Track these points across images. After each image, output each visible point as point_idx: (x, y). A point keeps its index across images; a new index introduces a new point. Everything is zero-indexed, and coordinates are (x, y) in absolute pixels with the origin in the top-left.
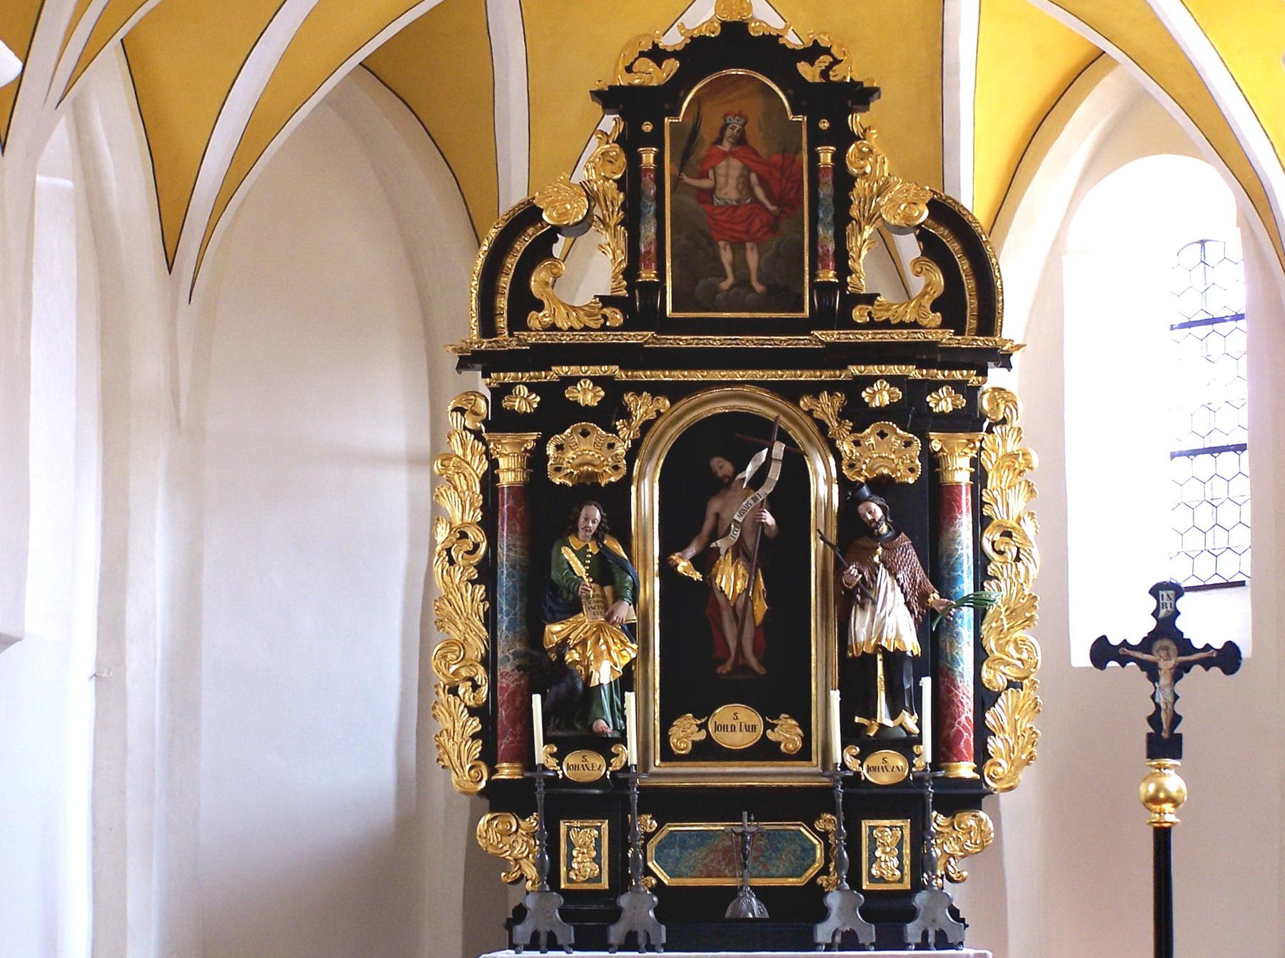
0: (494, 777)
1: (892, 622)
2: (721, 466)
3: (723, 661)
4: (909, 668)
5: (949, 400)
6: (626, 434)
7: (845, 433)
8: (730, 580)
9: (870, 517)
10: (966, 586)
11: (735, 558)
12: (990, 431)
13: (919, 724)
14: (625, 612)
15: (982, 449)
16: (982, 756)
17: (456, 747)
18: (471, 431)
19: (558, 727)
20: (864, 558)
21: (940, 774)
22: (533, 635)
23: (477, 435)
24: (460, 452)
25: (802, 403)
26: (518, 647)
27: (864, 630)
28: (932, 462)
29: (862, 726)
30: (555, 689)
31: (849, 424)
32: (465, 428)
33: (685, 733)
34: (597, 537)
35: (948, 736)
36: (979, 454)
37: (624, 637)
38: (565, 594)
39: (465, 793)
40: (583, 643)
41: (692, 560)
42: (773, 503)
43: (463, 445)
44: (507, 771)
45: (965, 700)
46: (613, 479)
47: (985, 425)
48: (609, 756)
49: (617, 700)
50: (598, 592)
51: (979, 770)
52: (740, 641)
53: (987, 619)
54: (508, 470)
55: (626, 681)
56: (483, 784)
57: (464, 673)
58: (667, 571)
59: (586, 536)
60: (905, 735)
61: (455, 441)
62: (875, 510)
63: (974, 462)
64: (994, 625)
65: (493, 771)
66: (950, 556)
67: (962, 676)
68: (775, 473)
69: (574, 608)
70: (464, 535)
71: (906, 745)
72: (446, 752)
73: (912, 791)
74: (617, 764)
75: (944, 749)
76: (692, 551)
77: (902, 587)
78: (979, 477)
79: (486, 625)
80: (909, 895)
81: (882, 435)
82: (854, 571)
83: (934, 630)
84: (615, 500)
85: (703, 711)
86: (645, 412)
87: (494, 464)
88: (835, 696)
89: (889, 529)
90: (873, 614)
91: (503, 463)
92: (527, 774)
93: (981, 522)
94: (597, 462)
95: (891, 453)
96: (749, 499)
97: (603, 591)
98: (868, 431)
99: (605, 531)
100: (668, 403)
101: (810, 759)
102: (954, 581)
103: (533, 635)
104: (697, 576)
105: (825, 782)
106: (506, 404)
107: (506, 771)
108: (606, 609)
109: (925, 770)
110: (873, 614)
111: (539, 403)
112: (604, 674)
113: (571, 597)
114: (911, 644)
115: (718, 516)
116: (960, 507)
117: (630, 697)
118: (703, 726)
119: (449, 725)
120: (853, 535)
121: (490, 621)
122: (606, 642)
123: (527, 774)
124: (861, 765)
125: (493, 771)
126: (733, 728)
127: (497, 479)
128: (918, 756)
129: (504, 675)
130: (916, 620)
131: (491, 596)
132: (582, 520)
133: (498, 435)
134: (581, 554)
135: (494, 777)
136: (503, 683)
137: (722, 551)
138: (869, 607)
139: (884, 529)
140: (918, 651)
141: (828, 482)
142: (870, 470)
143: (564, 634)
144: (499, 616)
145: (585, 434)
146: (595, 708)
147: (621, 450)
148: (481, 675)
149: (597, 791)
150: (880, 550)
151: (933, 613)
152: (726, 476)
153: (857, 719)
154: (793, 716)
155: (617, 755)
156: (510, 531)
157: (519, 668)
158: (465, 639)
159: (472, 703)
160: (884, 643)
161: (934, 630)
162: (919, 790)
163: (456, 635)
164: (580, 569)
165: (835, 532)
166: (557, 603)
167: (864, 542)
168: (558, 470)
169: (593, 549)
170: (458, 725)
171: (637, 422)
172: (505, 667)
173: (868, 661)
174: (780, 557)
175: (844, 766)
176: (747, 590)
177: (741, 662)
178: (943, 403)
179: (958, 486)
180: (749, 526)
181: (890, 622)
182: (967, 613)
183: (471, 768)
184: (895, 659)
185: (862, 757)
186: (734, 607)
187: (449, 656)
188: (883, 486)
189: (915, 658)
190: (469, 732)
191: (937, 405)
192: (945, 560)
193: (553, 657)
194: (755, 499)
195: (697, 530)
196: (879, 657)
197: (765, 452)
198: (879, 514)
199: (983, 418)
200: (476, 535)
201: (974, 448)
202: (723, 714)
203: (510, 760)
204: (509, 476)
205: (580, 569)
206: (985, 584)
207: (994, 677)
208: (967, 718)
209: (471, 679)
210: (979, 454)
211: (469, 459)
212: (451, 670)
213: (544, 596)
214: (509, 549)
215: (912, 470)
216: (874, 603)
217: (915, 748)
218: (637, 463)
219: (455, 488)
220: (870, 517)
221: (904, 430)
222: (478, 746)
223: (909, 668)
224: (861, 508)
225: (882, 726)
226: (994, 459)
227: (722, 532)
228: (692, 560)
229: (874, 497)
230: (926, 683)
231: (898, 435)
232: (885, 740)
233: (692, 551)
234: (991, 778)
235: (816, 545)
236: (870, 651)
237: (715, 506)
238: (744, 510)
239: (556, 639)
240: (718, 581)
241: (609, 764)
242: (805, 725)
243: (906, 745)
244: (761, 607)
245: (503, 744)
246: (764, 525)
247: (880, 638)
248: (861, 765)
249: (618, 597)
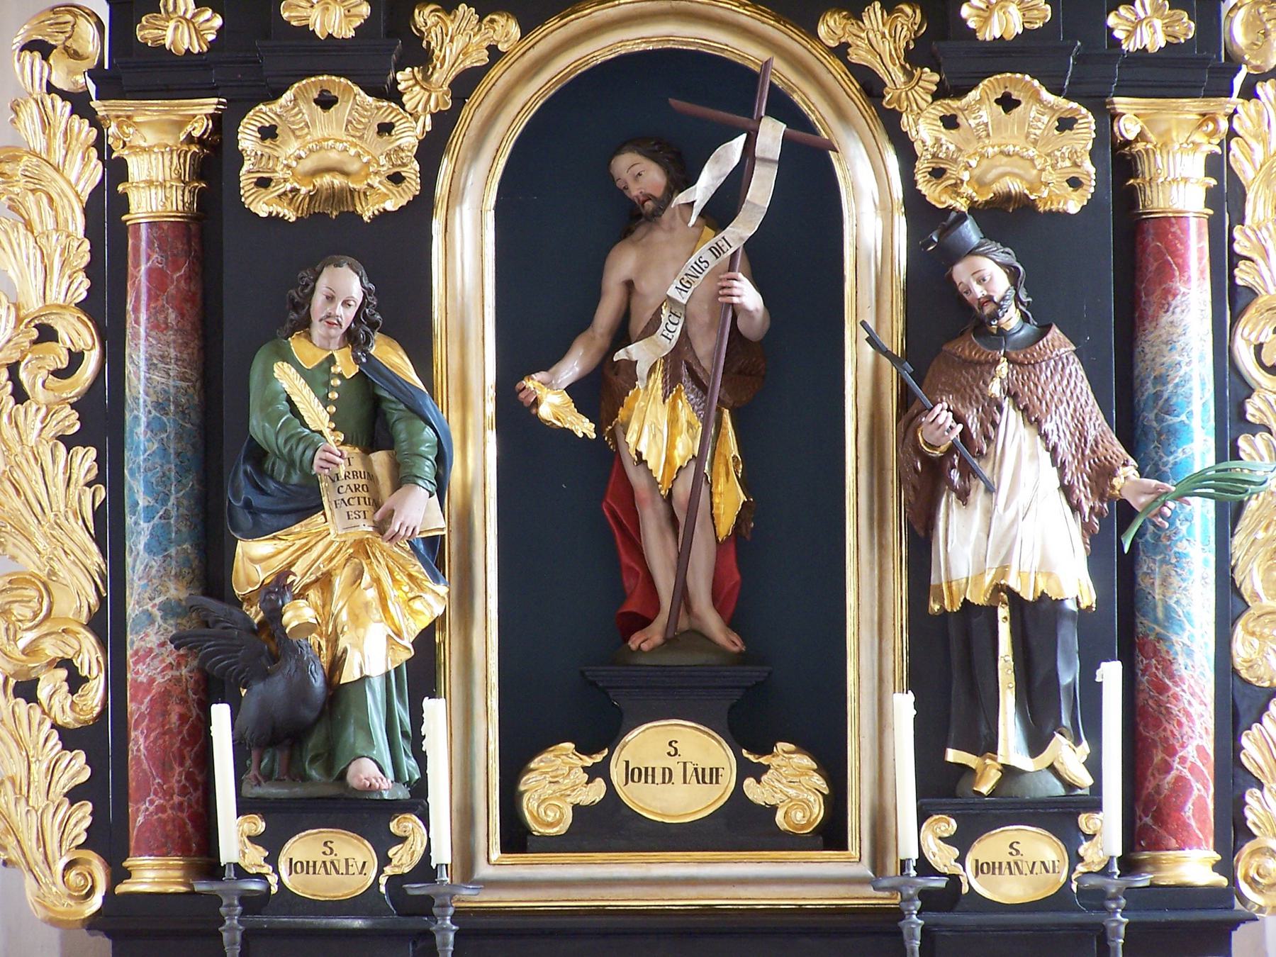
0: (121, 889)
1: (1021, 533)
2: (639, 174)
3: (643, 622)
4: (1069, 637)
5: (1158, 23)
6: (421, 96)
7: (923, 98)
8: (660, 433)
9: (979, 291)
10: (1197, 448)
11: (672, 381)
12: (1249, 92)
13: (1094, 764)
14: (420, 511)
15: (1232, 133)
16: (1233, 832)
17: (34, 819)
18: (65, 95)
19: (268, 777)
20: (966, 381)
21: (1143, 881)
22: (210, 569)
23: (79, 103)
24: (38, 143)
25: (822, 30)
26: (175, 592)
27: (968, 551)
28: (1120, 164)
29: (963, 769)
30: (259, 687)
31: (930, 78)
32: (51, 88)
33: (558, 784)
34: (354, 339)
35: (1158, 789)
36: (1226, 144)
37: (417, 569)
38: (281, 468)
39: (54, 922)
40: (325, 582)
41: (570, 390)
42: (760, 259)
43: (46, 124)
44: (149, 875)
45: (1195, 709)
46: (391, 206)
47: (1238, 81)
48: (383, 843)
49: (402, 713)
50: (357, 466)
51: (1225, 867)
52: (683, 572)
53: (1243, 523)
54: (150, 183)
55: (421, 673)
56: (96, 902)
57: (51, 649)
58: (515, 417)
59: (329, 338)
60: (1060, 790)
61: (30, 114)
62: (988, 275)
63: (1215, 165)
64: (1261, 535)
65: (118, 874)
66: (1161, 380)
67: (1190, 654)
68: (761, 190)
69: (304, 503)
70: (47, 334)
71: (1063, 815)
72: (11, 830)
73: (1075, 917)
74: (403, 859)
75: (1148, 823)
76: (571, 368)
77: (1054, 451)
78: (1227, 198)
79: (98, 539)
80: (394, 808)
81: (1008, 103)
82: (945, 418)
83: (1124, 549)
84: (396, 253)
85: (599, 735)
86: (464, 52)
87: (116, 170)
88: (904, 707)
89: (1025, 318)
90: (989, 514)
91: (137, 168)
92: (201, 887)
93: (1231, 300)
94: (354, 166)
95: (1027, 147)
96: (703, 252)
97: (368, 464)
98: (973, 95)
99: (373, 325)
100: (515, 31)
101: (842, 845)
102: (1169, 436)
103: (210, 569)
104: (584, 427)
105: (867, 897)
106: (146, 32)
107: (152, 875)
108: (377, 505)
109: (1105, 872)
110: (989, 514)
111: (220, 31)
112: (372, 655)
113: (295, 478)
114: (1074, 584)
115: (629, 285)
116: (1183, 268)
117: (434, 709)
118: (599, 772)
119: (18, 769)
120: (941, 326)
121: (109, 528)
122: (377, 581)
123: (201, 887)
124: (961, 860)
125: (118, 874)
126: (668, 775)
127: (122, 203)
128: (1090, 837)
129: (141, 657)
130: (1086, 527)
131: (111, 473)
132: (319, 299)
133: (127, 106)
134: (318, 378)
135: (121, 889)
136: (138, 672)
137: (642, 369)
138: (978, 497)
139: (1011, 319)
140: (1089, 598)
141: (885, 209)
142: (981, 183)
143: (277, 564)
144: (129, 520)
145: (326, 102)
146: (352, 734)
147: (409, 135)
148: (89, 654)
149: (358, 923)
150: (1003, 368)
151: (1126, 512)
152: (649, 197)
153: (952, 755)
154: (804, 746)
155: (402, 840)
156: (157, 326)
157: (178, 641)
158: (52, 572)
159: (68, 719)
160: (1013, 582)
161: (1124, 549)
162: (1093, 916)
163: (30, 563)
164: (317, 415)
165: (899, 326)
166: (263, 492)
167: (968, 348)
168: (263, 183)
169: (346, 366)
170: (39, 770)
171: (443, 75)
172: (148, 637)
173: (975, 620)
174: (773, 383)
175: (924, 867)
176: (698, 459)
177: (683, 624)
178: (1146, 31)
179: (1180, 218)
180: (702, 315)
181: (1025, 530)
182: (1202, 511)
183: (70, 865)
184: (1036, 618)
185: (962, 841)
186: (669, 498)
187: (17, 610)
188: (1008, 218)
189: (1083, 615)
190: (64, 782)
191: (1131, 34)
192: (1150, 389)
193: (255, 614)
194: (716, 251)
195: (584, 322)
196: (1003, 612)
197: (740, 141)
198: (1000, 284)
199: (1234, 64)
200: (77, 333)
201: (1216, 131)
202: (645, 743)
203: (160, 851)
204: (155, 192)
205: (317, 415)
206: (1241, 442)
207: (1264, 656)
208: (1200, 749)
209: (66, 663)
210: (1226, 144)
211: (57, 157)
212: (22, 644)
213: (231, 476)
214: (151, 366)
215: (1075, 183)
216: (990, 490)
217: (1082, 819)
218: (446, 166)
219: (28, 225)
220: (979, 291)
221: (1057, 91)
222: (83, 814)
223: (1069, 637)
224: (961, 272)
225: (1009, 772)
226: (1259, 156)
227: (638, 325)
228: (570, 390)
229: (992, 246)
230: (1111, 674)
231: (1042, 106)
232: (1012, 805)
233: (571, 368)
234: (1253, 883)
235: (858, 359)
236: (979, 598)
237: (623, 264)
238: (687, 274)
239: (262, 575)
240: (631, 438)
241: (384, 861)
242: (833, 767)
243: (1063, 815)
244: (729, 498)
245: (141, 814)
246: (736, 310)
247: (1003, 570)
248: (961, 860)
249: (402, 478)
